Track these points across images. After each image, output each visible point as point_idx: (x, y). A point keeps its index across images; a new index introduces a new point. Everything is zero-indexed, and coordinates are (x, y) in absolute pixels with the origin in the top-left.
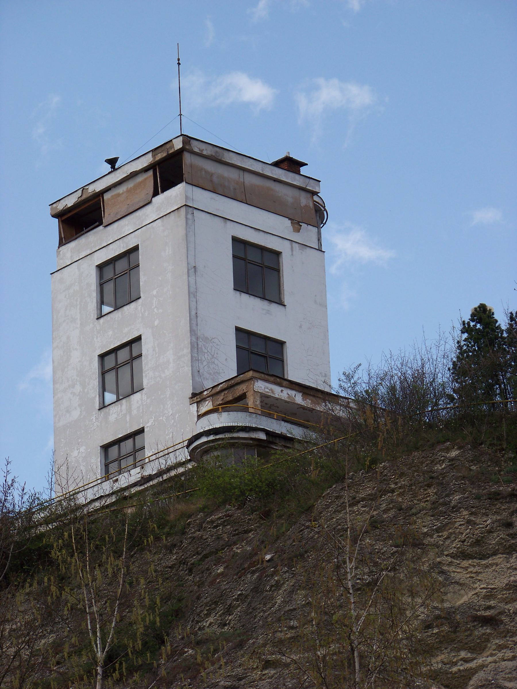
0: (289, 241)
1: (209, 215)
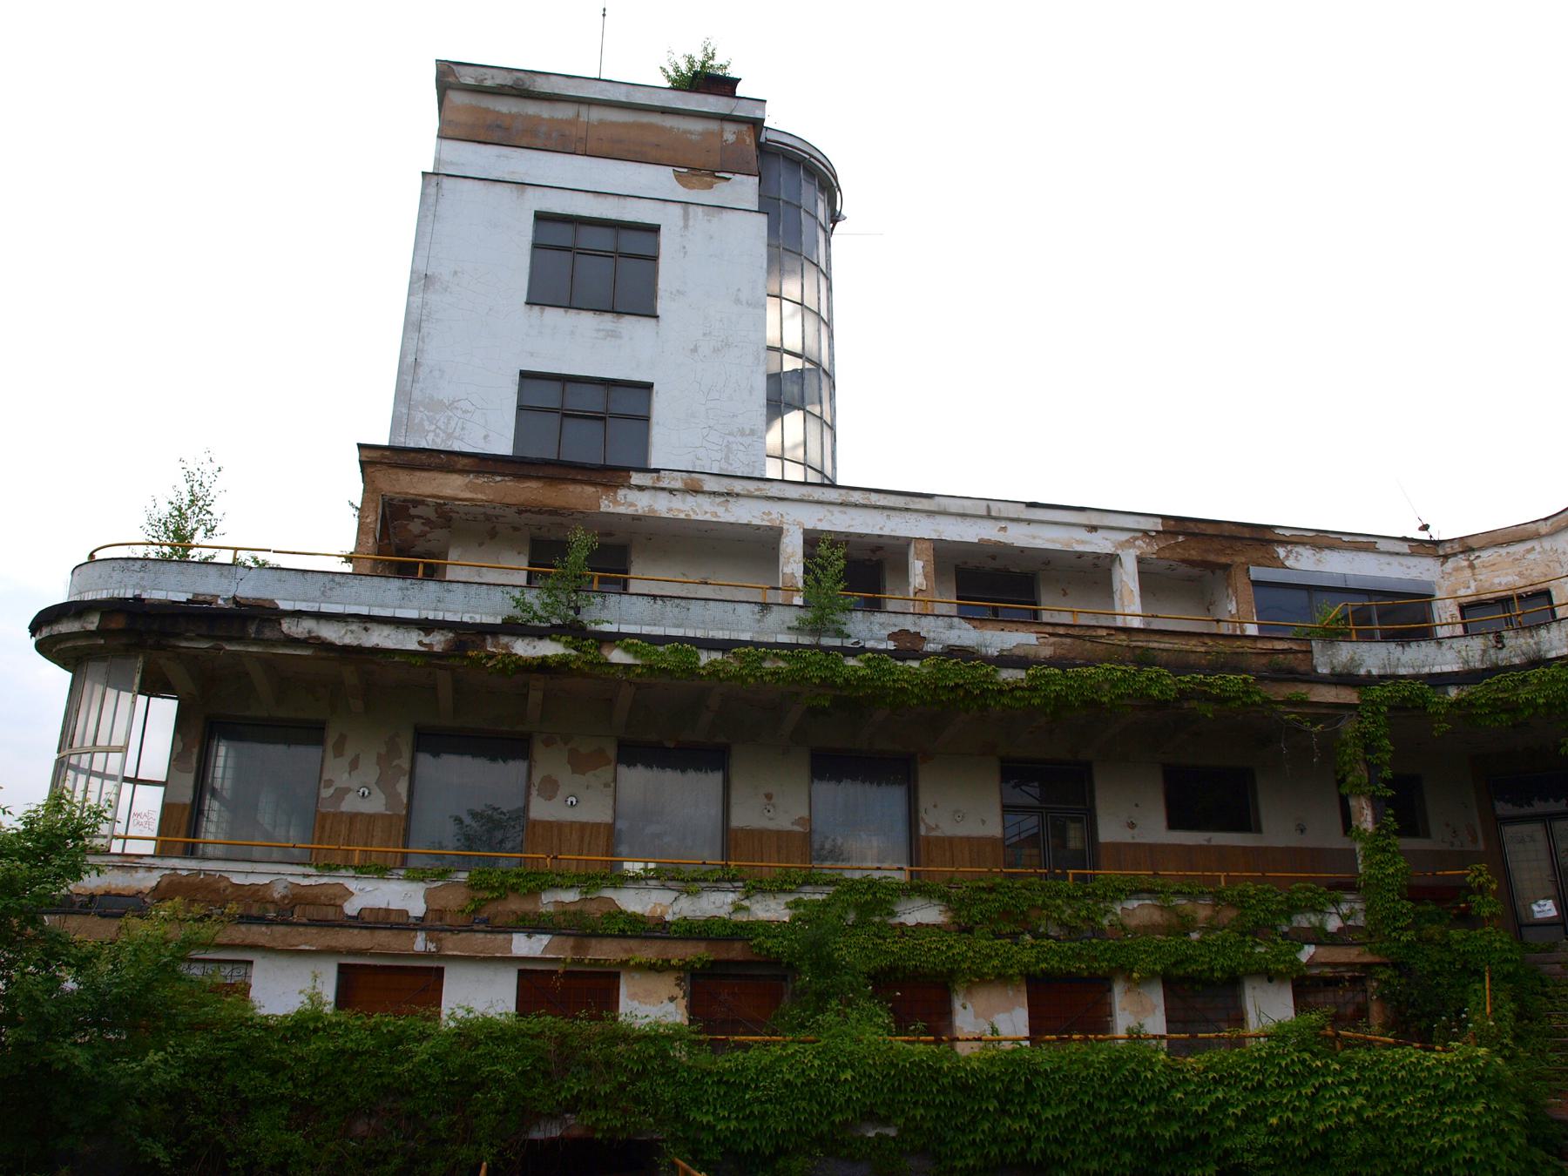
0: (679, 205)
1: (482, 183)
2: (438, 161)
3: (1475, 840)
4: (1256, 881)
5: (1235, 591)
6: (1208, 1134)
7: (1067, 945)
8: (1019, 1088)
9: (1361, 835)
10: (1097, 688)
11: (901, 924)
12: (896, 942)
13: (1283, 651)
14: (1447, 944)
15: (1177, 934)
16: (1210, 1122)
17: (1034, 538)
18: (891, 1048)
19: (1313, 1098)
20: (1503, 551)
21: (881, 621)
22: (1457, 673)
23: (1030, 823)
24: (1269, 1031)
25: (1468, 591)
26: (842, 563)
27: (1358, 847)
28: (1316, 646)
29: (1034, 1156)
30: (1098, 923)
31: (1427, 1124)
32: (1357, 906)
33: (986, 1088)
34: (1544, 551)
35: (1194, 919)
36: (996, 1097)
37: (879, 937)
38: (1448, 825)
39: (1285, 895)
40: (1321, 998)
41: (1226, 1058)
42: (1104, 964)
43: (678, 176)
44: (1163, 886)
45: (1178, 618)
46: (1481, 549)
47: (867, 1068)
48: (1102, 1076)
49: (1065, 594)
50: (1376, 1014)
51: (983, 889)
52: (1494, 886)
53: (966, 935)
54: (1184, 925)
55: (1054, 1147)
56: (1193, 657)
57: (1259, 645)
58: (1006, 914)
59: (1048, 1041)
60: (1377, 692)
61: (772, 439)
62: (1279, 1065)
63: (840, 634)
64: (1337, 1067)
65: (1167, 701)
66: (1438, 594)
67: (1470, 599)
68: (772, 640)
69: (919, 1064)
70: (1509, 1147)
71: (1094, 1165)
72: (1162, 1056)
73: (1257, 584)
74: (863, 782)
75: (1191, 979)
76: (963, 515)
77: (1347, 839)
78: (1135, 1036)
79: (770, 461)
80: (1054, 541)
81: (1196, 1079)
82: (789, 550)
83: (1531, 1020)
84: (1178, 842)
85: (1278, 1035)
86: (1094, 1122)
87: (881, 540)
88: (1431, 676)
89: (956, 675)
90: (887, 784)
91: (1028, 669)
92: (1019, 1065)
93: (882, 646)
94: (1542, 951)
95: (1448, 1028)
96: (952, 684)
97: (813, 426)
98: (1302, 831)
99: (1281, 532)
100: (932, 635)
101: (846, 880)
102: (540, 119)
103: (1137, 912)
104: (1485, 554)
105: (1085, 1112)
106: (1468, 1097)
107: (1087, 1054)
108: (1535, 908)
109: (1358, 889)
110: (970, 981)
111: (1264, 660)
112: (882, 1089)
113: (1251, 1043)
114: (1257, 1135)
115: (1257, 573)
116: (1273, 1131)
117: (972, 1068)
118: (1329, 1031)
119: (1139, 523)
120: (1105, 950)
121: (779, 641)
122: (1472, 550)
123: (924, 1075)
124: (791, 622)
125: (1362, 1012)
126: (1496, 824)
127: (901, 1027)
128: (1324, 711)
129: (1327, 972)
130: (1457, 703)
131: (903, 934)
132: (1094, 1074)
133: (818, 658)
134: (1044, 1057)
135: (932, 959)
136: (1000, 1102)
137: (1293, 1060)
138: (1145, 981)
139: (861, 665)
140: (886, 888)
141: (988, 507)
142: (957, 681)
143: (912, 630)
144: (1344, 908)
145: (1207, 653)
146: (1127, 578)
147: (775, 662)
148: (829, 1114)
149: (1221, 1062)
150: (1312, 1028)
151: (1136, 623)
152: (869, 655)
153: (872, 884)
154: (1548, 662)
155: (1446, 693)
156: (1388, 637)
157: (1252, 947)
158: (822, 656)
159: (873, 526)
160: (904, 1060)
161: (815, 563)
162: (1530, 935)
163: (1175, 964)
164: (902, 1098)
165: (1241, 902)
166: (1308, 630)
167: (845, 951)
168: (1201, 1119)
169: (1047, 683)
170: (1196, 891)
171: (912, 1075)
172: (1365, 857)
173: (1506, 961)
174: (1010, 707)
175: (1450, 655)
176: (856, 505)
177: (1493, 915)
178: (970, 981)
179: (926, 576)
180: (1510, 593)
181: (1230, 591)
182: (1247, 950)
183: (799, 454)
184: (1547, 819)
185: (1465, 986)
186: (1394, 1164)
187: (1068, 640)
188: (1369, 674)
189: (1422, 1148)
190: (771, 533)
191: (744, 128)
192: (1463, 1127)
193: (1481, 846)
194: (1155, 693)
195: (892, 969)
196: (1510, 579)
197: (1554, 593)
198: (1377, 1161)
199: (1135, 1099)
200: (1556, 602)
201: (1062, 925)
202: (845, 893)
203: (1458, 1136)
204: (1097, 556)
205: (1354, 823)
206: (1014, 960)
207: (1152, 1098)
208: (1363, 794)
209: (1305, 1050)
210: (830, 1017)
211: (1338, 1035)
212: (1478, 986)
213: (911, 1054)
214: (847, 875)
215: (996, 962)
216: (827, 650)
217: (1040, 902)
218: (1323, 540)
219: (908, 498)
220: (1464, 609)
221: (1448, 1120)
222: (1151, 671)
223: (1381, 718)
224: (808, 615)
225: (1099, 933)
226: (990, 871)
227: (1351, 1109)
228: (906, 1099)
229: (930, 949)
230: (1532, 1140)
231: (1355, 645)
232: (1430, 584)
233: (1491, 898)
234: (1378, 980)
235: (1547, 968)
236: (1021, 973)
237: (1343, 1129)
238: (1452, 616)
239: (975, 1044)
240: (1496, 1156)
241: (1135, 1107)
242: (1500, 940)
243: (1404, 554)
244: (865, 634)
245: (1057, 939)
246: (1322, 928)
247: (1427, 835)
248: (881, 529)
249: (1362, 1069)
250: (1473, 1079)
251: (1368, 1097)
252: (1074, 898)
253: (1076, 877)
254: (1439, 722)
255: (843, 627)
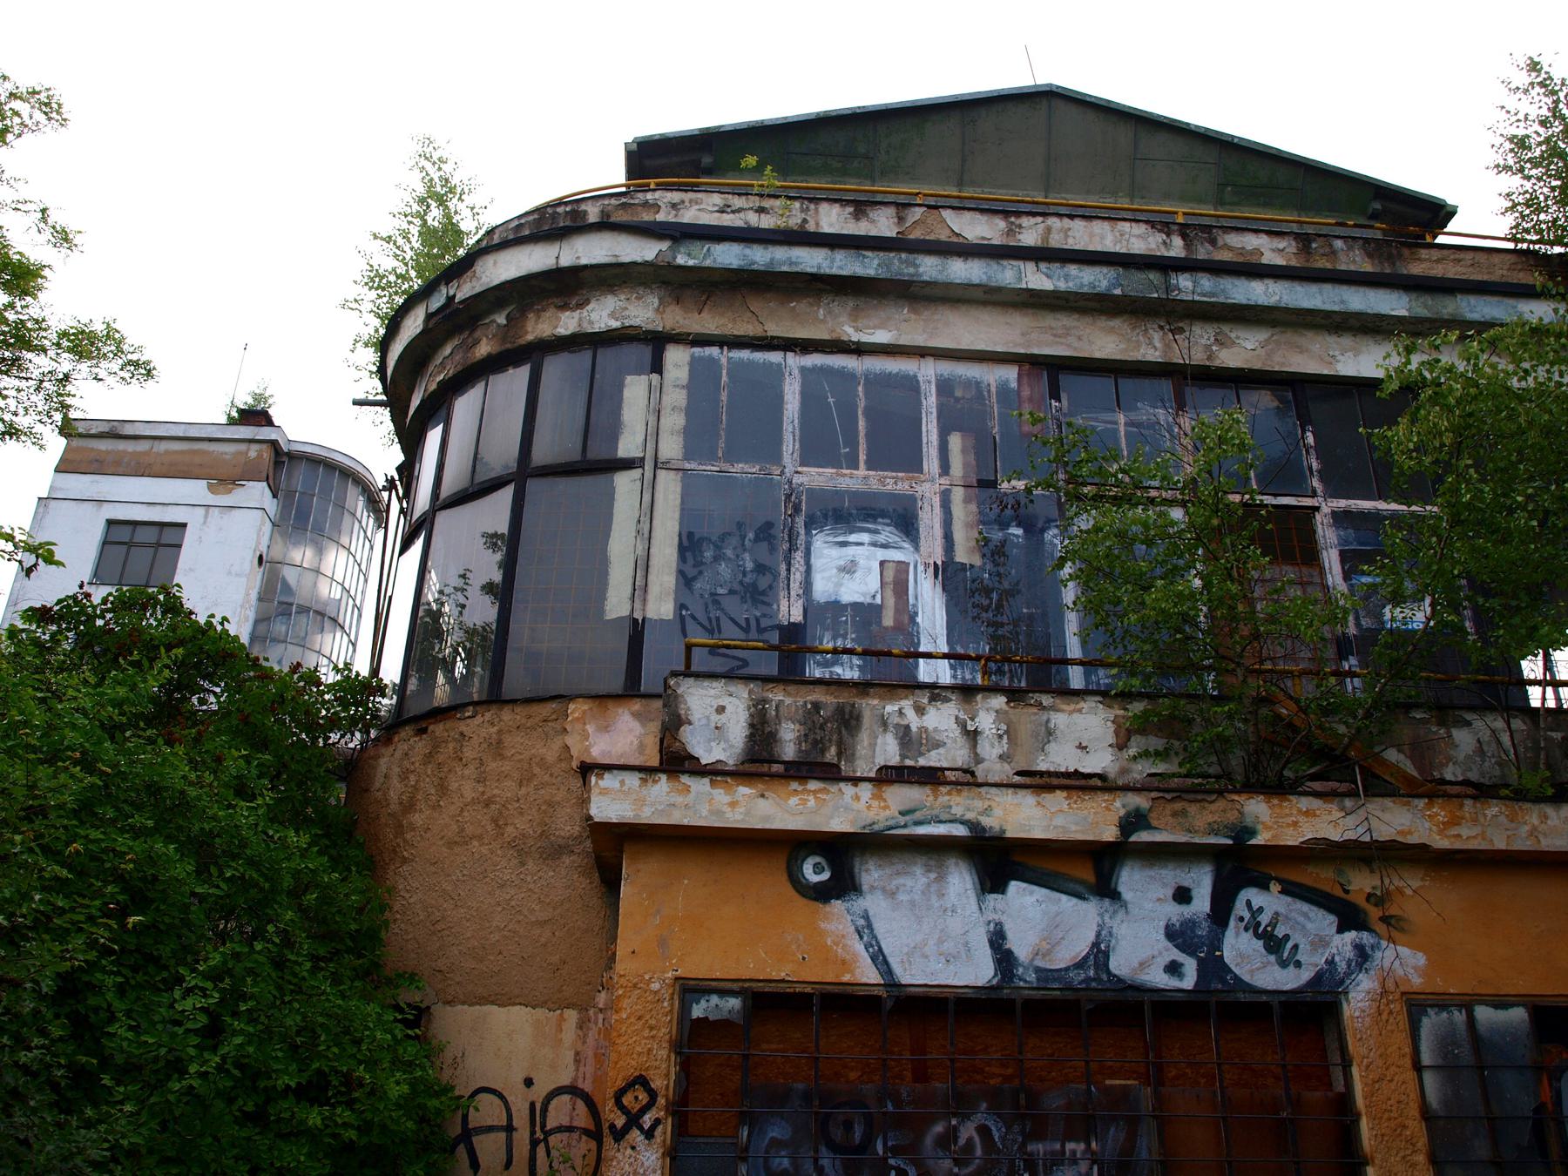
2: (52, 488)
43: (210, 487)
102: (125, 452)
191: (264, 446)
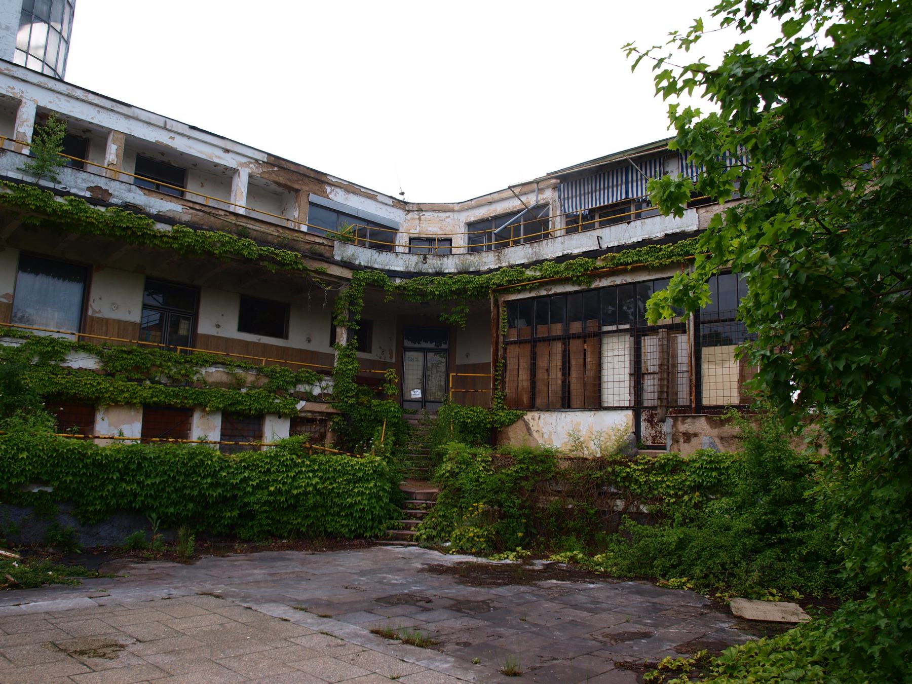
3: (391, 357)
4: (281, 364)
5: (299, 206)
6: (237, 495)
7: (171, 389)
8: (133, 467)
9: (339, 348)
10: (213, 245)
11: (69, 367)
12: (64, 378)
13: (319, 244)
14: (370, 406)
15: (235, 389)
16: (239, 489)
17: (191, 148)
18: (56, 440)
19: (294, 478)
20: (436, 214)
21: (84, 177)
22: (402, 272)
23: (155, 317)
24: (277, 443)
25: (415, 232)
26: (62, 135)
27: (336, 353)
28: (337, 244)
29: (137, 505)
30: (191, 378)
31: (346, 492)
32: (330, 383)
33: (113, 466)
34: (454, 219)
35: (245, 381)
36: (119, 471)
37: (53, 374)
38: (380, 348)
39: (295, 374)
40: (303, 428)
41: (252, 456)
42: (191, 401)
44: (231, 361)
45: (267, 213)
46: (426, 211)
47: (38, 451)
48: (183, 462)
49: (202, 186)
50: (329, 439)
51: (124, 352)
52: (396, 380)
53: (110, 377)
54: (239, 384)
55: (149, 500)
56: (270, 237)
57: (307, 237)
58: (137, 368)
59: (154, 442)
60: (362, 275)
61: (22, 36)
62: (280, 460)
63: (54, 180)
64: (308, 463)
65: (251, 259)
66: (401, 230)
67: (415, 235)
68: (5, 174)
69: (72, 451)
70: (381, 503)
71: (172, 510)
72: (218, 453)
73: (312, 204)
74: (54, 277)
75: (238, 413)
76: (149, 123)
77: (332, 349)
78: (203, 442)
79: (17, 53)
80: (201, 152)
81: (235, 466)
82: (25, 117)
83: (400, 445)
84: (242, 338)
85: (281, 446)
86: (174, 487)
87: (91, 126)
88: (389, 271)
89: (128, 221)
90: (69, 281)
91: (173, 226)
92: (135, 454)
93: (82, 194)
94: (411, 413)
95: (362, 447)
96: (124, 226)
97: (54, 37)
98: (309, 341)
99: (330, 178)
100: (116, 193)
101: (35, 337)
103: (214, 374)
104: (427, 214)
105: (171, 481)
106: (368, 479)
107: (176, 449)
108: (412, 393)
109: (332, 375)
110: (109, 404)
111: (308, 246)
112: (46, 464)
113: (265, 449)
114: (263, 496)
115: (313, 198)
116: (271, 494)
117: (106, 455)
118: (308, 445)
119: (254, 154)
120: (193, 393)
121: (9, 175)
122: (422, 210)
123: (75, 457)
124: (20, 165)
125: (322, 437)
126: (402, 350)
127: (61, 430)
128: (334, 280)
129: (309, 415)
130: (399, 287)
131: (69, 374)
132: (179, 461)
133: (36, 193)
134: (150, 450)
135: (86, 390)
136: (120, 474)
137: (287, 459)
138: (212, 412)
139: (66, 203)
140: (61, 344)
141: (165, 122)
142: (128, 224)
143: (104, 187)
144: (324, 384)
145: (278, 236)
146: (241, 184)
147: (4, 189)
148: (9, 478)
149: (249, 458)
150: (299, 443)
151: (241, 211)
152: (72, 197)
153: (53, 341)
154: (444, 274)
155: (395, 281)
156: (373, 247)
157: (273, 399)
158: (39, 191)
159: (88, 115)
160: (63, 448)
161: (44, 130)
162: (407, 406)
163: (230, 405)
164: (59, 470)
165: (271, 375)
166: (334, 235)
167: (28, 380)
168: (234, 487)
169: (184, 236)
170: (248, 366)
171: (67, 456)
172: (339, 359)
173: (395, 417)
174: (159, 247)
175: (401, 262)
176: (77, 99)
177: (393, 394)
178: (109, 404)
179: (117, 156)
180: (434, 236)
181: (297, 205)
182: (271, 400)
183: (40, 54)
184: (425, 351)
185: (373, 427)
186: (327, 511)
187: (201, 214)
188: (360, 265)
189: (342, 503)
190: (12, 101)
192: (363, 494)
193: (394, 360)
194: (246, 253)
195: (60, 394)
196: (436, 229)
197: (453, 241)
198: (320, 509)
199: (200, 475)
200: (453, 245)
201: (170, 377)
202: (33, 344)
203: (360, 498)
204: (226, 168)
205: (337, 341)
206: (138, 395)
207: (209, 475)
208: (344, 326)
209: (293, 454)
210: (16, 420)
211: (311, 447)
212: (379, 428)
213: (68, 444)
214: (36, 333)
215: (126, 395)
216: (43, 189)
217: (158, 363)
218: (351, 188)
219: (114, 104)
220: (411, 240)
221: (356, 490)
222: (246, 241)
223: (361, 288)
224: (34, 163)
225: (190, 383)
226: (130, 341)
227: (312, 484)
228: (61, 471)
229: (86, 384)
230: (391, 500)
231: (356, 247)
232: (398, 224)
233: (394, 386)
234: (333, 421)
235: (411, 421)
236: (141, 402)
237: (306, 493)
238: (406, 242)
239: (109, 441)
240: (375, 507)
241: (199, 479)
242: (394, 406)
243: (389, 205)
244: (71, 183)
245: (165, 385)
246: (311, 393)
247: (370, 352)
248: (92, 118)
249: (321, 464)
250: (371, 471)
251: (321, 478)
252: (180, 363)
253: (182, 351)
254: (388, 295)
255: (57, 176)
